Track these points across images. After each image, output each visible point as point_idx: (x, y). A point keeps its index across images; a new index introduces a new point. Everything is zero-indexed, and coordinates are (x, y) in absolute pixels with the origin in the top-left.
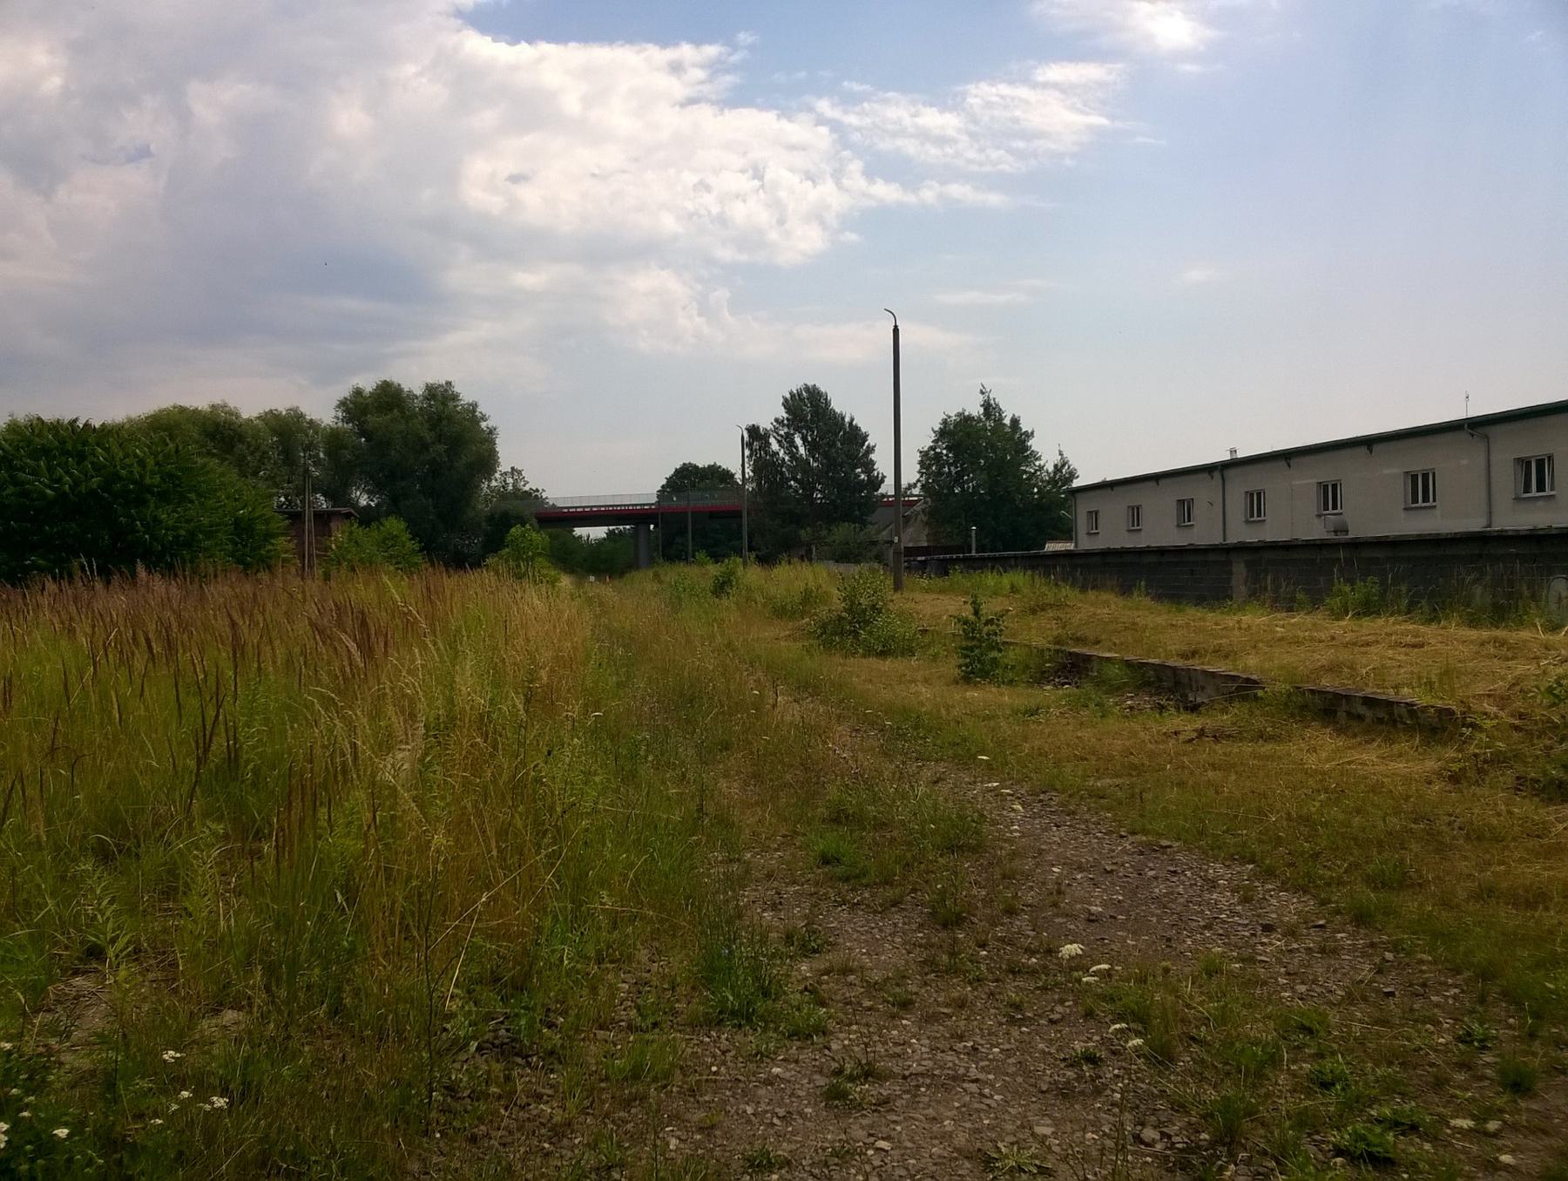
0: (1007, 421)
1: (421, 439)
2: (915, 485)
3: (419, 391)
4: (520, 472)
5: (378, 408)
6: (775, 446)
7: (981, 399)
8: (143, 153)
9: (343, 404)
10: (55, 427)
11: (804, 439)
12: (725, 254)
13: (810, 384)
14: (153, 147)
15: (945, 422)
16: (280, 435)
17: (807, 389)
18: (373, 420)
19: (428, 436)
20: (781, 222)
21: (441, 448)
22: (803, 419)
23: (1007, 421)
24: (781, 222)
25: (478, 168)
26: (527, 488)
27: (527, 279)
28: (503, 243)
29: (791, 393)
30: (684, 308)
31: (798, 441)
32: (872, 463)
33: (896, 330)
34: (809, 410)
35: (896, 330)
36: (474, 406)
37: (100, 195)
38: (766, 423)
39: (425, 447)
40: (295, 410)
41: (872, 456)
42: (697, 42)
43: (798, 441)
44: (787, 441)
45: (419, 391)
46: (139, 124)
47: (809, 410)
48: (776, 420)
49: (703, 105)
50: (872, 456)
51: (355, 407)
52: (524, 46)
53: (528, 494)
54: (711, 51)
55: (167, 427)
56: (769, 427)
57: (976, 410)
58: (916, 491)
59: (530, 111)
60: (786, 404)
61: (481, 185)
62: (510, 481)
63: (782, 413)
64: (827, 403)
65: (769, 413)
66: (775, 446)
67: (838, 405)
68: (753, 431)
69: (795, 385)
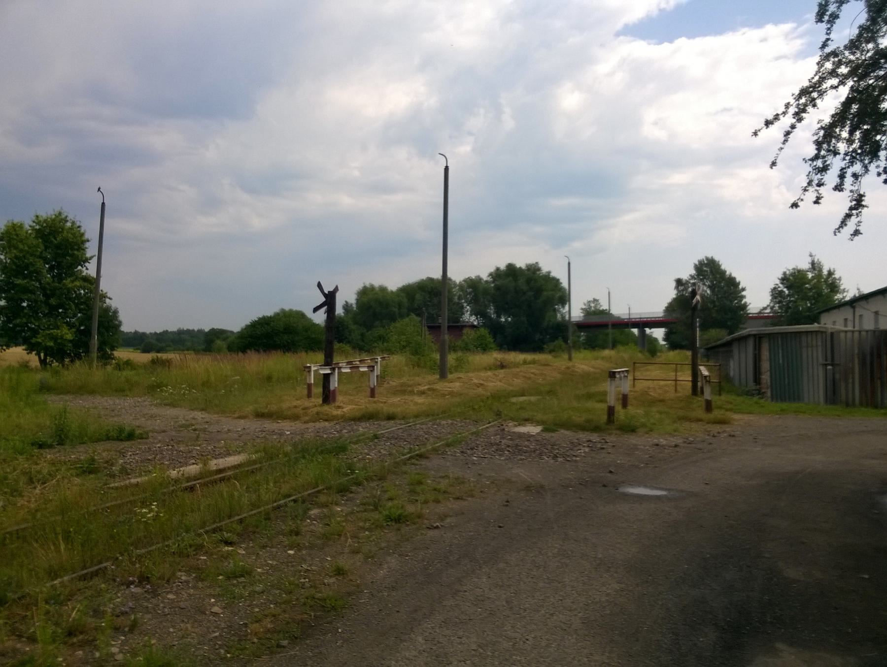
0: (825, 272)
4: (597, 301)
7: (809, 260)
10: (247, 327)
13: (710, 256)
15: (785, 273)
17: (707, 259)
21: (530, 293)
23: (825, 272)
25: (650, 115)
27: (678, 178)
28: (670, 158)
34: (709, 269)
35: (569, 264)
36: (549, 272)
42: (776, 23)
47: (709, 269)
50: (744, 293)
51: (497, 275)
52: (666, 44)
54: (787, 27)
57: (805, 265)
59: (673, 82)
62: (592, 305)
63: (693, 272)
65: (687, 272)
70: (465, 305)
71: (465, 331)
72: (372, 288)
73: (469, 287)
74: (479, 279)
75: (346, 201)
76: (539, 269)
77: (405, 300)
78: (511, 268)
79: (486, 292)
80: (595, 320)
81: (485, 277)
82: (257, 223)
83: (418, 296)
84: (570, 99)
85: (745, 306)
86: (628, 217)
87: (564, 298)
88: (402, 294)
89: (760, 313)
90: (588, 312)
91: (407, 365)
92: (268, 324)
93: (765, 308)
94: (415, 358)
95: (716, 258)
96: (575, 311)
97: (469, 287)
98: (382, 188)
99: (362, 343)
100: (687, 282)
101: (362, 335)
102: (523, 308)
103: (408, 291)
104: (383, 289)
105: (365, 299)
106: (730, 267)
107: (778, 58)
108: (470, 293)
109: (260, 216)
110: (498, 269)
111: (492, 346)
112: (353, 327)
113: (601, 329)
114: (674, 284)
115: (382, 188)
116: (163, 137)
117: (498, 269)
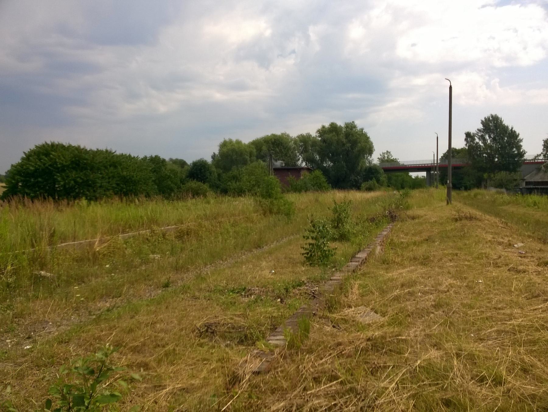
1: (342, 142)
2: (540, 155)
3: (343, 125)
4: (390, 153)
5: (331, 131)
6: (477, 140)
8: (294, 52)
9: (318, 131)
11: (490, 137)
12: (499, 64)
13: (494, 114)
14: (296, 50)
16: (303, 142)
17: (492, 116)
18: (327, 136)
19: (344, 140)
20: (525, 48)
21: (349, 145)
22: (490, 129)
24: (525, 48)
26: (392, 158)
27: (419, 81)
29: (485, 118)
30: (480, 87)
31: (487, 137)
32: (521, 146)
33: (451, 88)
34: (493, 125)
35: (451, 88)
36: (362, 129)
37: (283, 68)
38: (473, 131)
39: (344, 145)
40: (309, 134)
41: (521, 144)
43: (487, 137)
44: (482, 138)
45: (343, 125)
46: (296, 44)
47: (493, 125)
48: (478, 130)
49: (487, 7)
50: (521, 144)
51: (323, 132)
53: (393, 160)
55: (28, 157)
56: (475, 132)
58: (541, 157)
60: (482, 123)
61: (403, 51)
62: (386, 156)
63: (481, 127)
64: (501, 122)
66: (477, 140)
67: (506, 122)
68: (468, 135)
69: (487, 114)
70: (298, 154)
71: (302, 173)
72: (231, 141)
73: (301, 141)
74: (309, 136)
75: (218, 96)
76: (355, 127)
77: (255, 150)
78: (334, 128)
79: (314, 143)
80: (388, 165)
81: (314, 133)
82: (162, 109)
83: (264, 148)
84: (356, 32)
85: (521, 154)
86: (389, 105)
87: (370, 151)
88: (253, 146)
89: (535, 159)
90: (382, 160)
91: (256, 211)
92: (47, 154)
93: (538, 156)
94: (267, 202)
95: (500, 116)
96: (375, 159)
97: (301, 141)
98: (240, 87)
99: (218, 183)
100: (474, 135)
101: (219, 175)
102: (341, 157)
103: (257, 144)
104: (239, 142)
105: (225, 150)
106: (508, 122)
107: (484, 6)
108: (301, 146)
109: (163, 104)
110: (323, 127)
111: (326, 185)
112: (214, 169)
113: (394, 174)
114: (464, 136)
115: (240, 87)
116: (103, 56)
117: (323, 127)
